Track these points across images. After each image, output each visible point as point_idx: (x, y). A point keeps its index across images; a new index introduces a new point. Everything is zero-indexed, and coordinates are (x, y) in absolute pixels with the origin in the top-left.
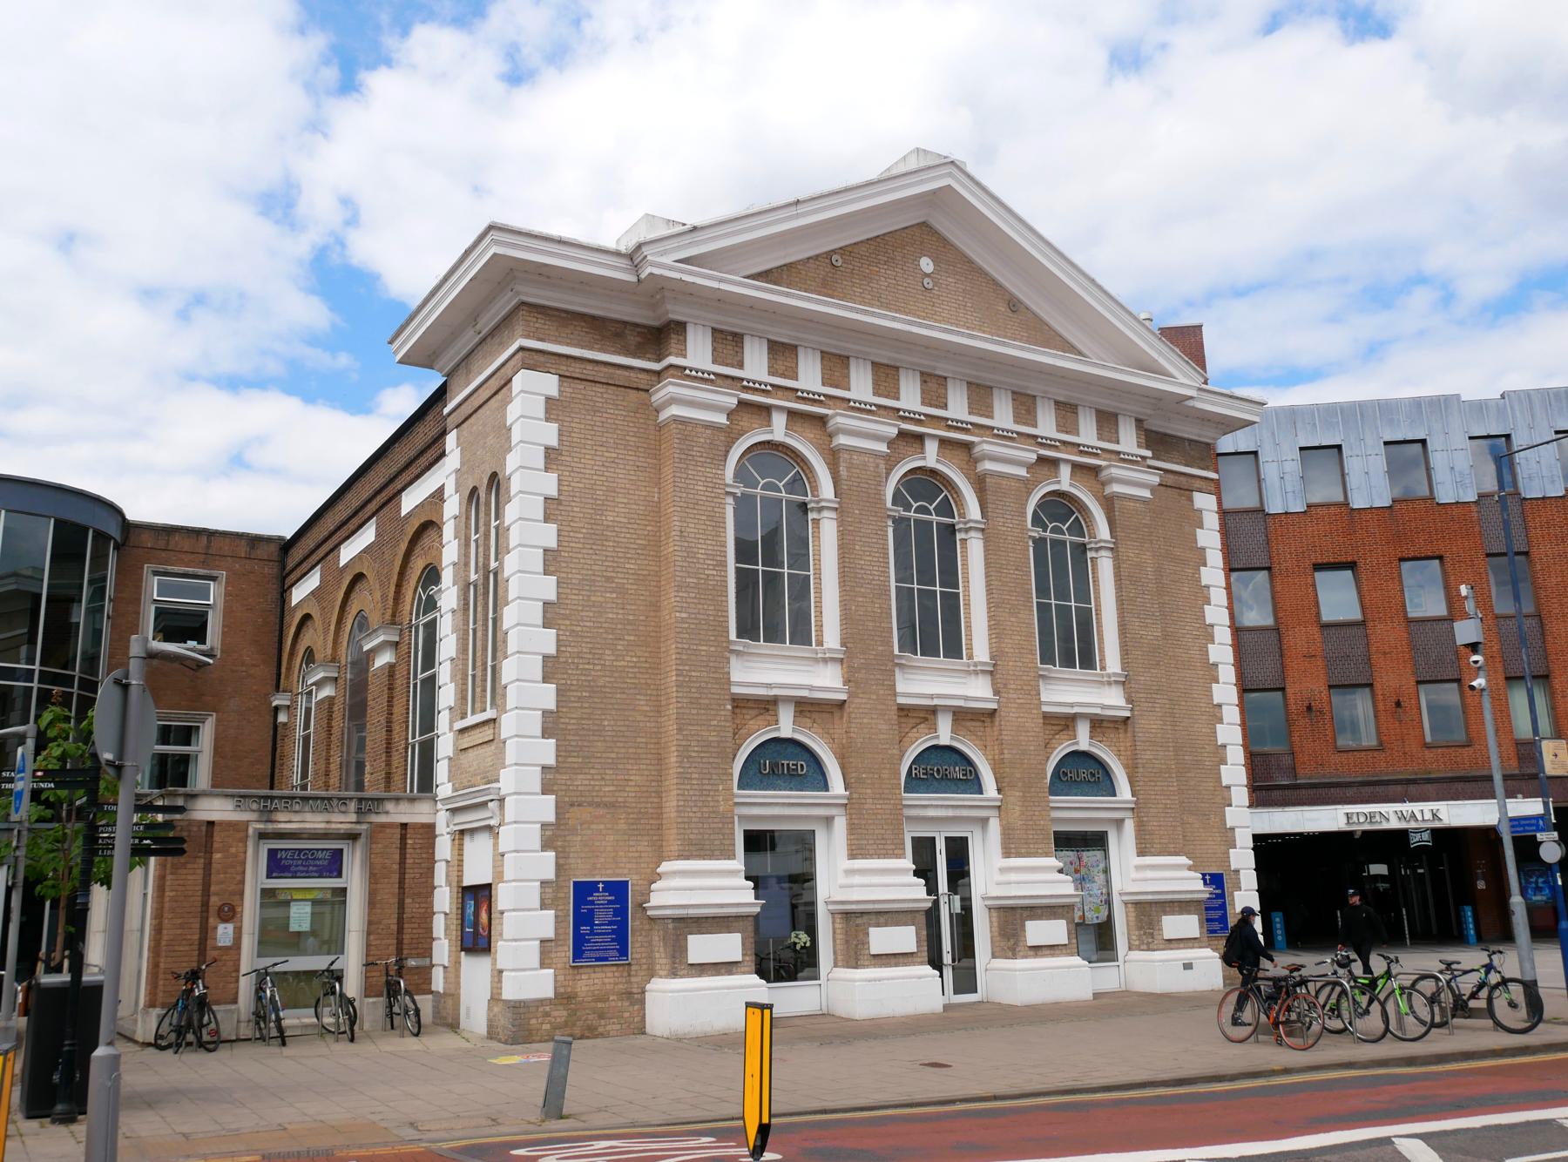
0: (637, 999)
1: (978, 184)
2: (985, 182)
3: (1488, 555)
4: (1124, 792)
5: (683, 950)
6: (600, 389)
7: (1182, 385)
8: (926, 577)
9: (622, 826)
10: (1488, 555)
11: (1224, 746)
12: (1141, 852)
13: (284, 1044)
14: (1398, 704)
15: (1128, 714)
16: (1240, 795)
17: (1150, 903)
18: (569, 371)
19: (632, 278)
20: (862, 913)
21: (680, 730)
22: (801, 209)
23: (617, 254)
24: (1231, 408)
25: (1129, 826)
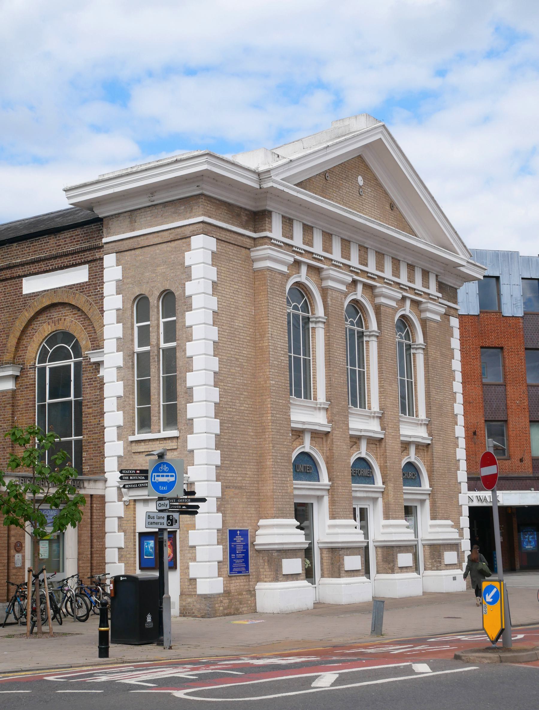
0: (252, 593)
1: (392, 138)
2: (396, 139)
3: (526, 349)
4: (426, 485)
5: (279, 567)
6: (232, 247)
7: (462, 259)
8: (297, 351)
9: (245, 500)
10: (526, 349)
11: (459, 460)
12: (433, 518)
13: (61, 624)
14: (475, 433)
15: (429, 442)
16: (464, 487)
17: (440, 545)
18: (224, 239)
19: (257, 186)
20: (343, 548)
21: (273, 447)
22: (329, 150)
23: (254, 172)
24: (473, 271)
25: (326, 500)
